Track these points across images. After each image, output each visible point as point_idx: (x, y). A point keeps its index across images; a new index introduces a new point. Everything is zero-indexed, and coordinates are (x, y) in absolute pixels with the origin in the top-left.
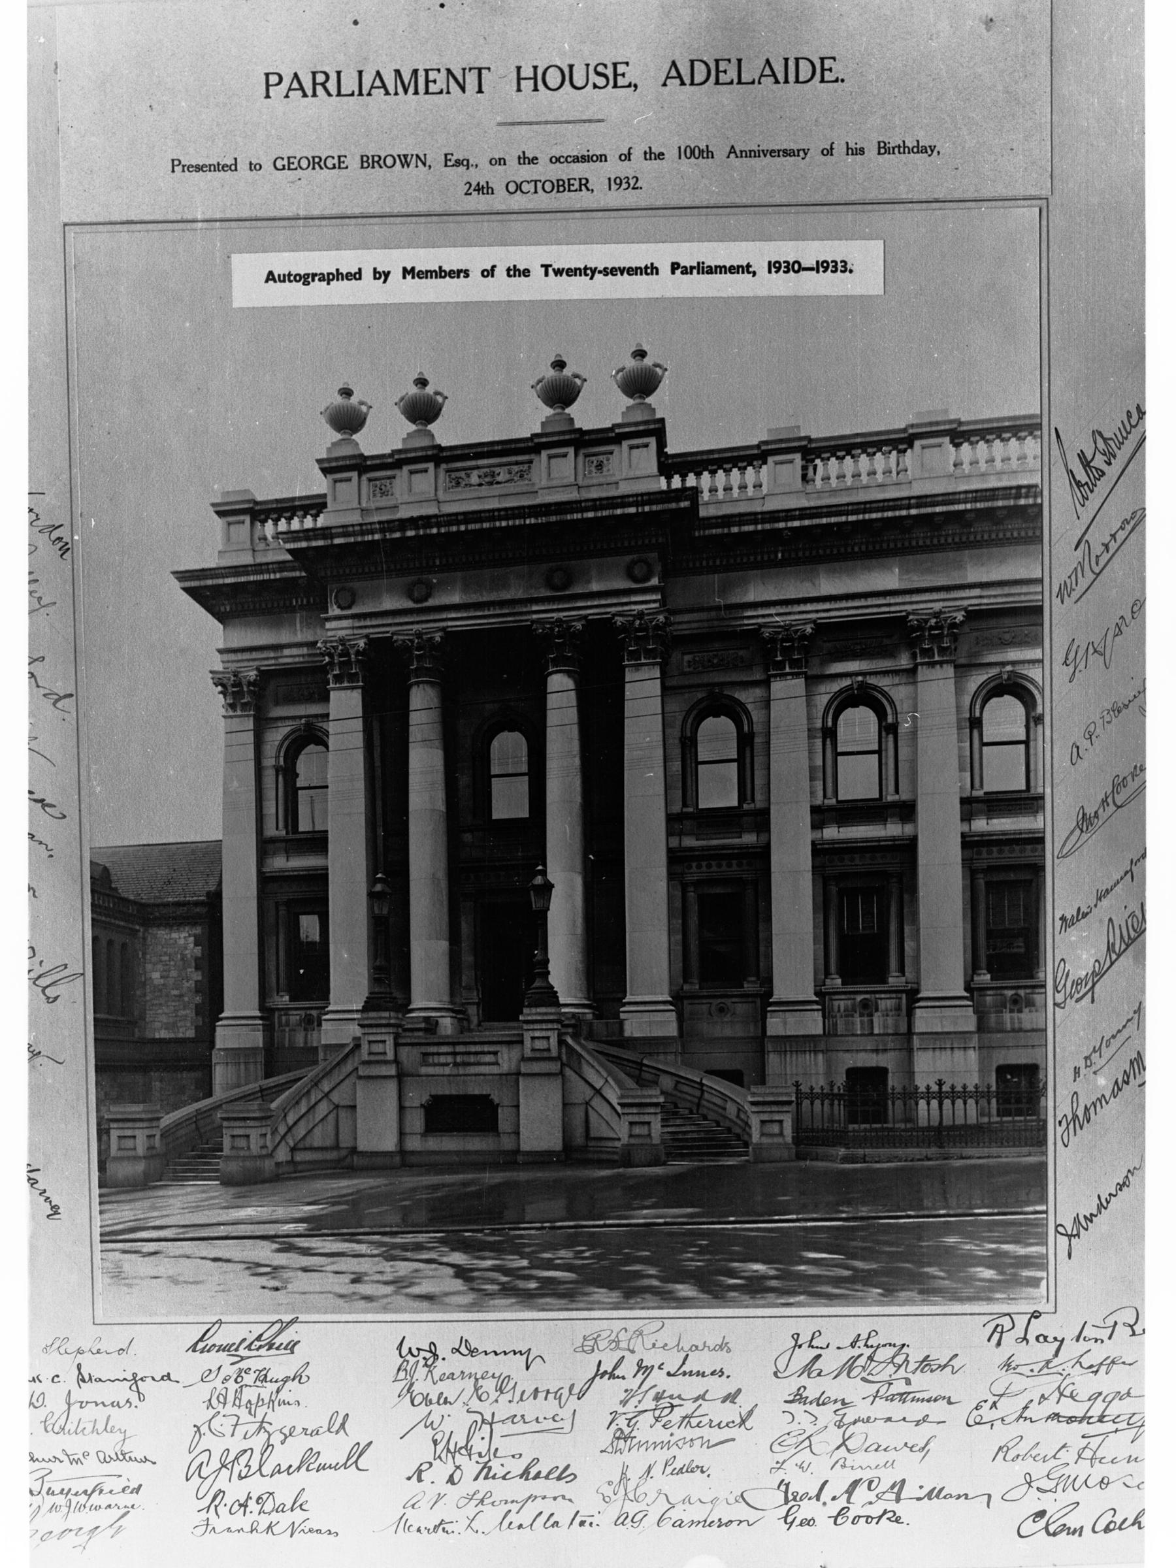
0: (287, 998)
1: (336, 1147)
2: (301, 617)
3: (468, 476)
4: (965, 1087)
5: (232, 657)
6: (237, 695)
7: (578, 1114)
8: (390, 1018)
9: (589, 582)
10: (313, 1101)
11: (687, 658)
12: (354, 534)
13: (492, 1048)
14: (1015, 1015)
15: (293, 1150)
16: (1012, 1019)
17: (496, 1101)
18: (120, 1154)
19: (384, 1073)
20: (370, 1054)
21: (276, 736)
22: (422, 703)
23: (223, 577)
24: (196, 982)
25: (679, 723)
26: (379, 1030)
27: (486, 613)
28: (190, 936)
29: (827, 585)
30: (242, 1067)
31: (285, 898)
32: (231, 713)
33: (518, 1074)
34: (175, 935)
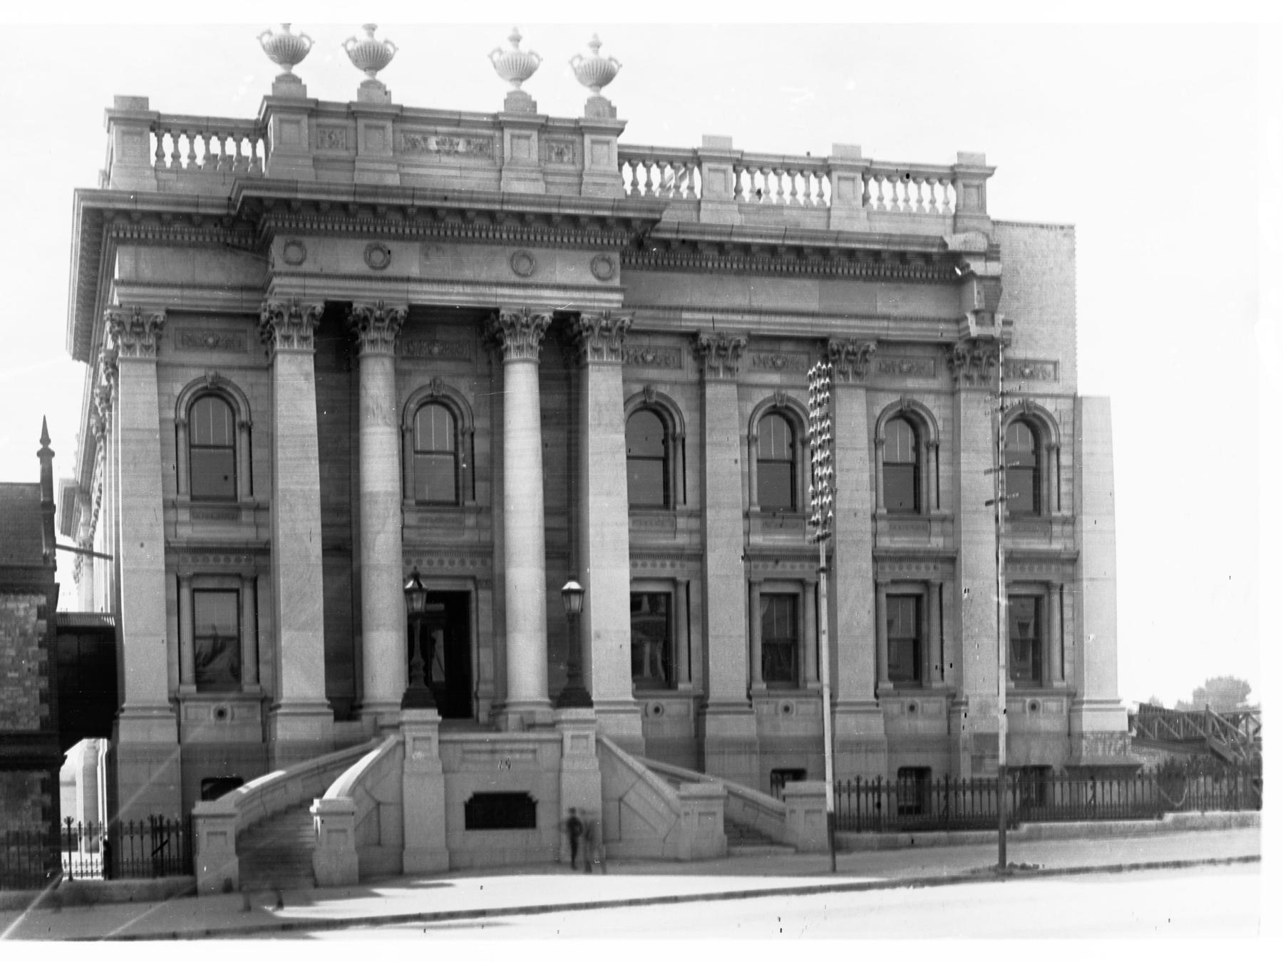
3: (425, 140)
13: (531, 746)
22: (377, 382)
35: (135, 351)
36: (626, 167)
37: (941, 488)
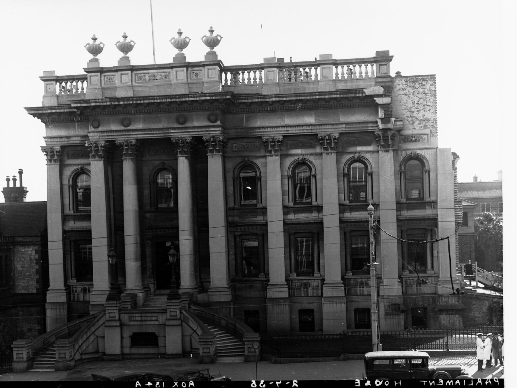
0: (76, 281)
1: (97, 352)
2: (78, 125)
3: (145, 76)
5: (49, 140)
6: (52, 156)
7: (188, 339)
8: (116, 304)
9: (193, 121)
10: (88, 335)
11: (235, 145)
12: (99, 102)
14: (362, 289)
15: (81, 354)
16: (360, 290)
17: (157, 335)
18: (18, 360)
19: (115, 325)
20: (110, 317)
21: (68, 172)
22: (128, 168)
23: (45, 110)
24: (36, 269)
25: (232, 171)
26: (113, 308)
27: (153, 132)
28: (33, 250)
29: (288, 121)
30: (58, 310)
31: (73, 239)
32: (49, 163)
33: (165, 325)
34: (27, 249)
36: (223, 74)
37: (343, 195)
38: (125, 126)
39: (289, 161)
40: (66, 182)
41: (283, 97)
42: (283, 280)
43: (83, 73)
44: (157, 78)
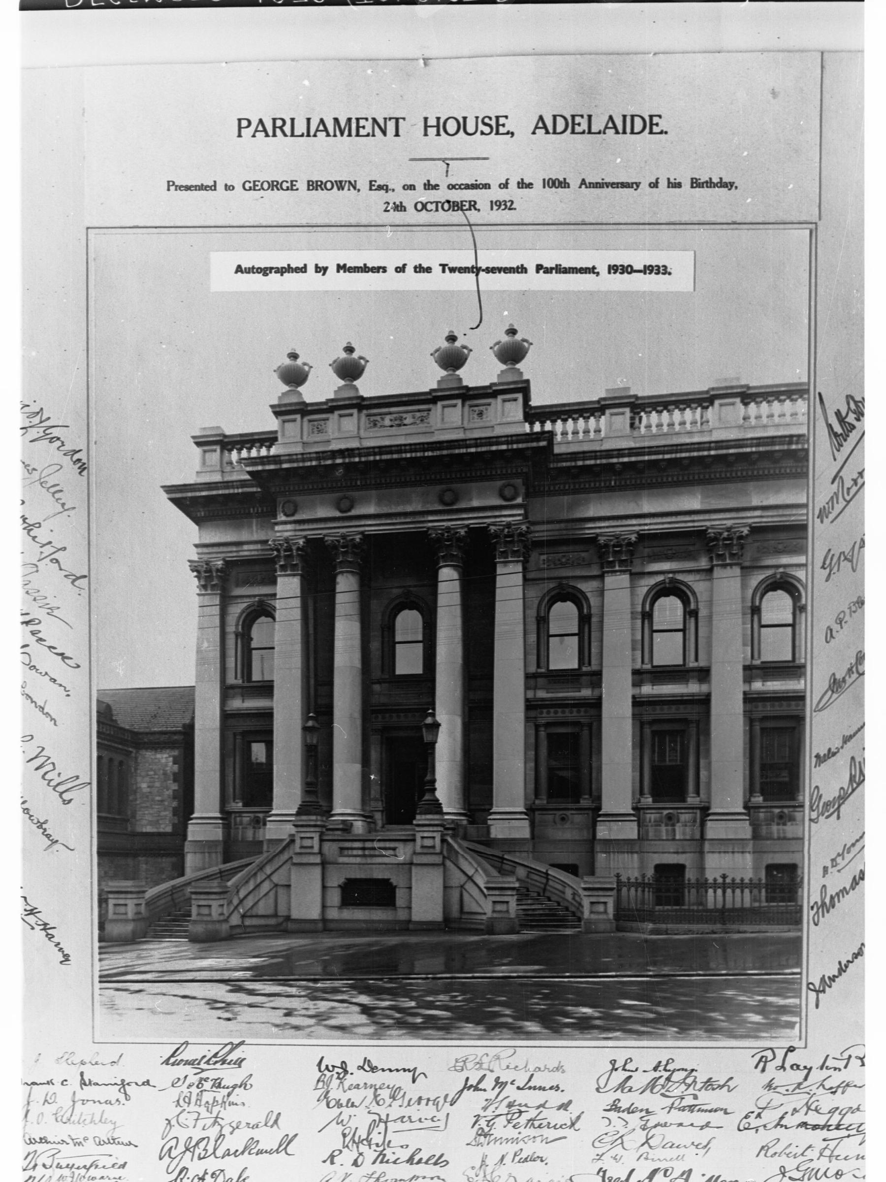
3: (383, 419)
4: (742, 880)
5: (205, 550)
6: (209, 579)
7: (455, 895)
9: (471, 500)
10: (259, 881)
11: (544, 557)
13: (392, 845)
14: (781, 827)
15: (243, 916)
17: (395, 884)
18: (115, 917)
21: (236, 610)
25: (535, 606)
28: (170, 756)
33: (411, 864)
34: (159, 756)
35: (615, 566)
38: (341, 511)
39: (646, 584)
40: (231, 629)
41: (643, 454)
42: (626, 807)
43: (271, 424)
44: (406, 422)
